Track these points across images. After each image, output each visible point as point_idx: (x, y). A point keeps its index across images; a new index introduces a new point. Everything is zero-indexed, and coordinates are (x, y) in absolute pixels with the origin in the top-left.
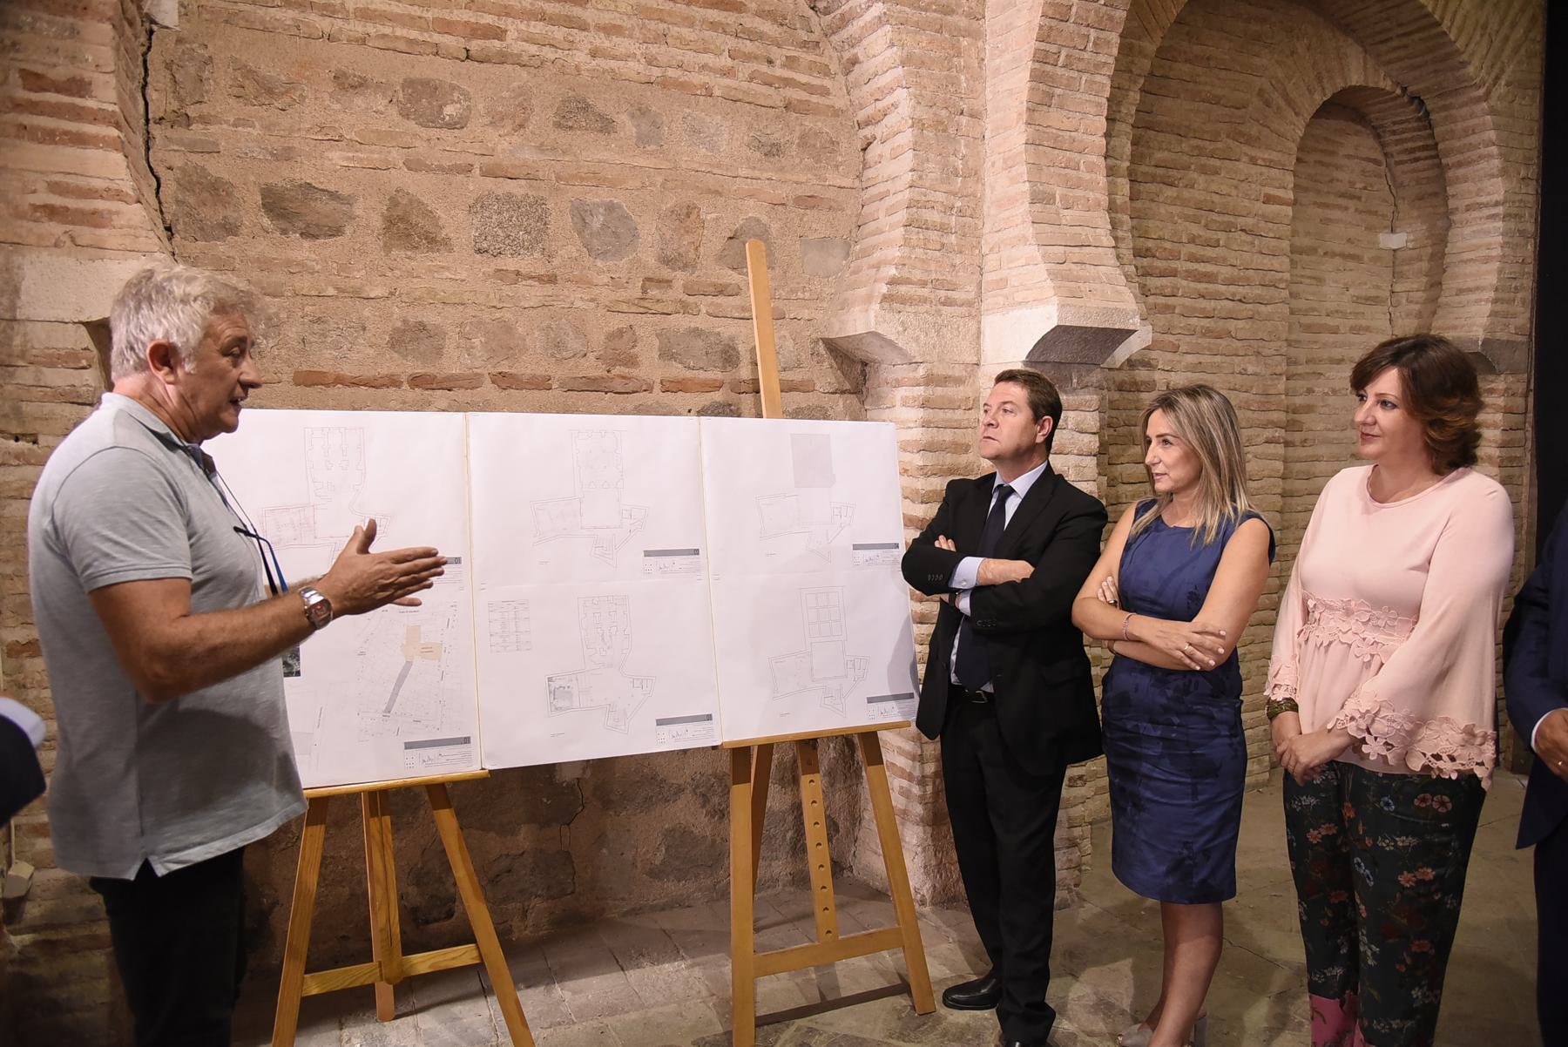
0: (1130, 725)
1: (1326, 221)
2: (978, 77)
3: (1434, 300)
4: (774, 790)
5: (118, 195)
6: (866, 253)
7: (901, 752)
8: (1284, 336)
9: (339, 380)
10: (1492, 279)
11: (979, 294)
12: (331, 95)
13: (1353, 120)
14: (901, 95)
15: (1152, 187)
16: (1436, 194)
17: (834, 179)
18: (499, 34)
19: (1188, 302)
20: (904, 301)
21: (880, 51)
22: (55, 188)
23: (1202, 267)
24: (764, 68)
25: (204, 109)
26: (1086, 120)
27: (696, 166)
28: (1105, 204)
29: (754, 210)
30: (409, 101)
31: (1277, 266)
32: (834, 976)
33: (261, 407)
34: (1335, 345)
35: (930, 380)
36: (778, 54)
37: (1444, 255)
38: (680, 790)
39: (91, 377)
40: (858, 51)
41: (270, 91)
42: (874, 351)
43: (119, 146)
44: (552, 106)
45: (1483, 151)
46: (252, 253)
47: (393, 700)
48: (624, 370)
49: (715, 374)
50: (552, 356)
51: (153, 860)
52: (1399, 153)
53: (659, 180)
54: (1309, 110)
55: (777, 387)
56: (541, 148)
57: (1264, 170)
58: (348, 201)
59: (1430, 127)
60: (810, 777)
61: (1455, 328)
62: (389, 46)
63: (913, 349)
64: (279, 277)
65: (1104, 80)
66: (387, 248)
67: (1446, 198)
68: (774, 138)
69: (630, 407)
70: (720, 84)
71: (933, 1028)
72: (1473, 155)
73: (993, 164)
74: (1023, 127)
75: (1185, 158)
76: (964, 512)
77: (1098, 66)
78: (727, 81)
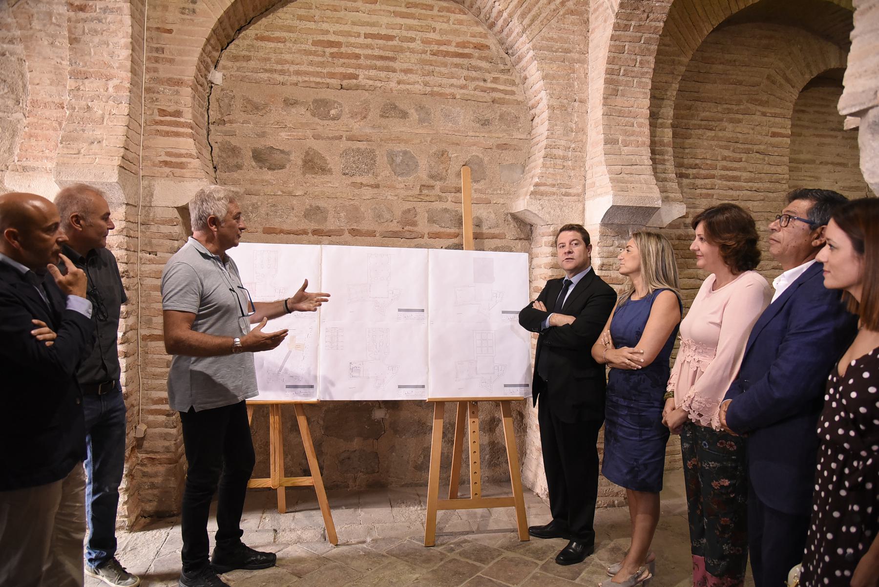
0: (615, 399)
5: (191, 156)
9: (282, 231)
14: (543, 93)
15: (700, 132)
17: (517, 135)
18: (356, 77)
19: (721, 192)
20: (542, 194)
21: (534, 72)
22: (168, 154)
23: (730, 173)
24: (482, 84)
25: (231, 117)
27: (447, 132)
29: (475, 151)
31: (780, 171)
39: (178, 230)
41: (257, 108)
43: (192, 136)
46: (248, 177)
53: (429, 139)
55: (471, 236)
56: (373, 127)
57: (771, 119)
58: (288, 154)
60: (473, 420)
62: (307, 85)
64: (258, 187)
65: (648, 81)
66: (304, 174)
75: (720, 115)
77: (643, 74)
78: (463, 91)
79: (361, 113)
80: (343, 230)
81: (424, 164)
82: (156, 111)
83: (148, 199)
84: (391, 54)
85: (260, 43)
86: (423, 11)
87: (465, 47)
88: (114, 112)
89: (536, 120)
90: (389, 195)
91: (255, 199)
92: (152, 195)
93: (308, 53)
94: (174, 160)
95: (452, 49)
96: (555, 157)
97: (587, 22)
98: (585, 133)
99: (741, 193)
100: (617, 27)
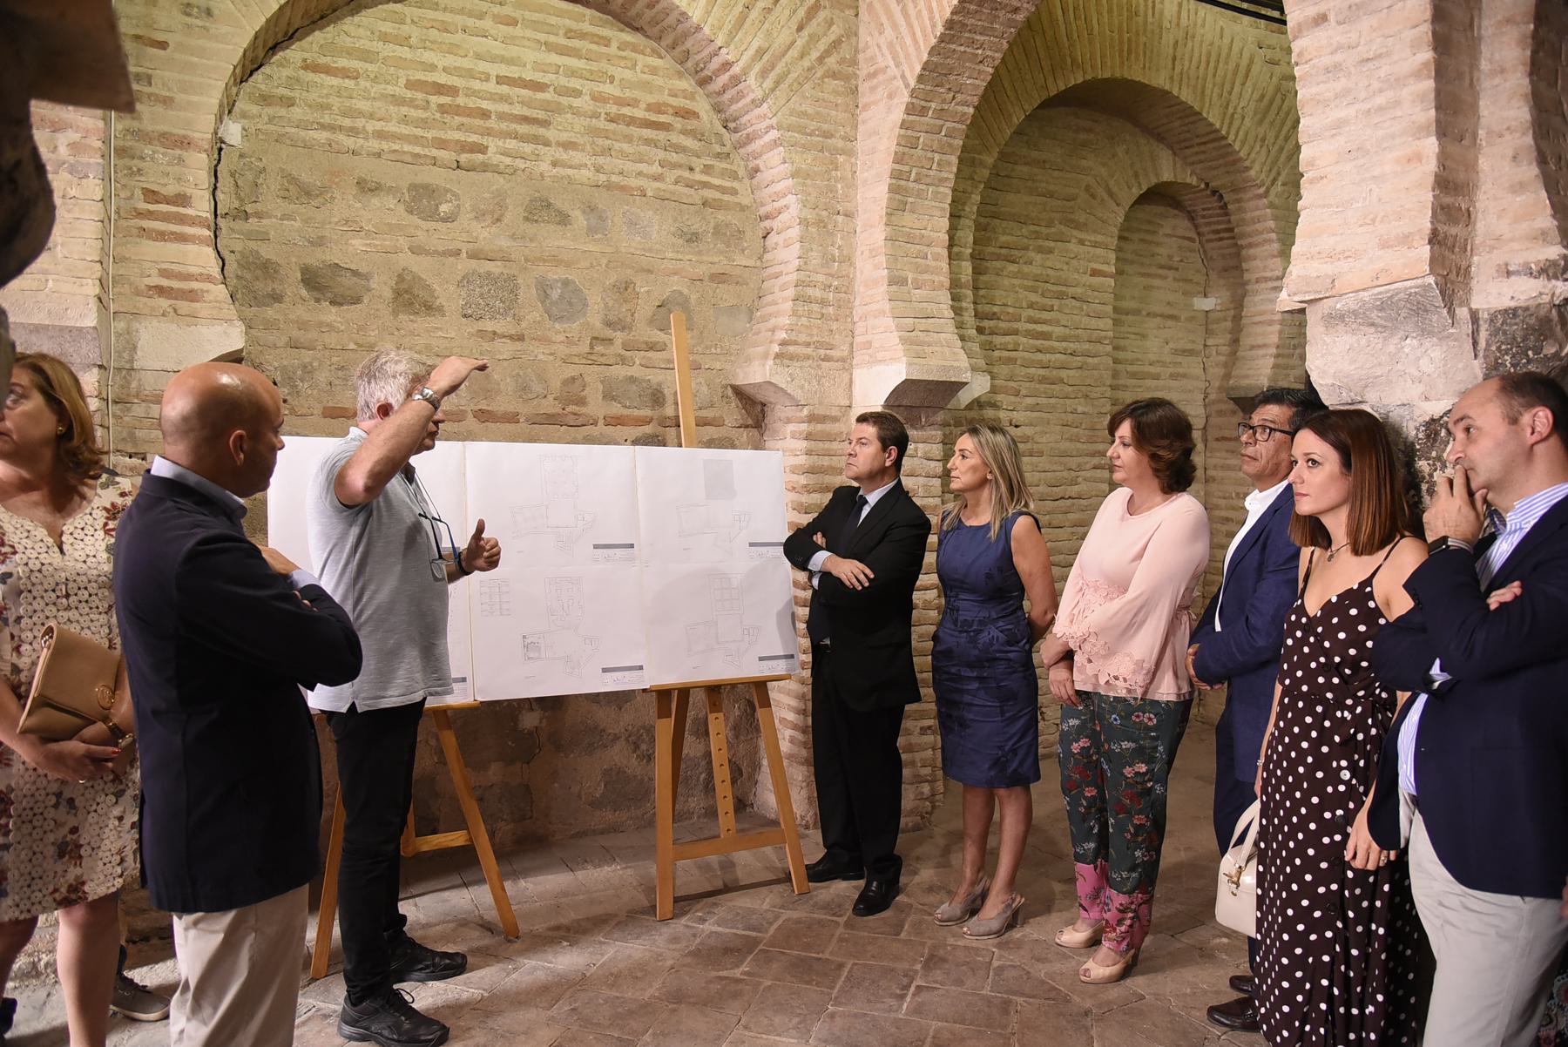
0: (953, 670)
1: (1148, 288)
2: (851, 185)
3: (1234, 353)
4: (689, 739)
5: (209, 279)
6: (764, 319)
7: (790, 708)
10: (1274, 339)
11: (851, 352)
15: (998, 264)
17: (741, 260)
21: (775, 166)
22: (164, 273)
23: (1039, 328)
24: (686, 174)
25: (259, 206)
28: (947, 284)
29: (677, 284)
31: (1101, 326)
33: (298, 434)
35: (812, 419)
36: (698, 163)
38: (616, 738)
41: (308, 194)
45: (1266, 236)
49: (646, 412)
53: (604, 261)
56: (513, 237)
58: (366, 277)
59: (1227, 214)
61: (1247, 377)
62: (398, 158)
63: (799, 395)
64: (313, 335)
65: (947, 191)
66: (395, 313)
69: (580, 437)
70: (651, 187)
72: (1259, 239)
76: (834, 521)
78: (657, 185)
79: (492, 212)
81: (596, 301)
82: (138, 192)
83: (126, 355)
84: (541, 115)
85: (310, 76)
86: (594, 47)
87: (660, 112)
88: (72, 193)
90: (540, 352)
91: (307, 356)
92: (135, 348)
93: (399, 101)
94: (175, 284)
95: (640, 113)
96: (808, 300)
97: (854, 91)
99: (1053, 357)
100: (910, 109)
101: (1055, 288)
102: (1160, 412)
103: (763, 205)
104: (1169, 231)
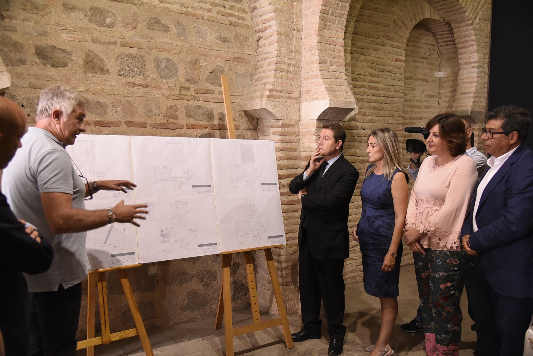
1: (416, 67)
2: (300, 17)
6: (259, 79)
8: (402, 110)
10: (474, 89)
12: (62, 11)
13: (426, 30)
14: (273, 23)
16: (455, 58)
20: (275, 97)
24: (222, 9)
26: (338, 34)
27: (198, 45)
28: (344, 64)
29: (219, 62)
30: (92, 15)
31: (399, 84)
32: (256, 339)
34: (419, 113)
35: (284, 126)
37: (457, 80)
40: (257, 4)
41: (37, 8)
42: (263, 115)
44: (146, 20)
45: (471, 43)
46: (32, 72)
47: (107, 239)
48: (173, 121)
49: (205, 123)
50: (147, 115)
51: (63, 284)
52: (442, 42)
53: (185, 50)
54: (411, 28)
56: (142, 36)
57: (395, 49)
58: (70, 53)
59: (453, 33)
61: (461, 106)
63: (277, 115)
64: (42, 82)
66: (85, 72)
67: (458, 60)
68: (227, 35)
69: (176, 134)
70: (207, 15)
71: (294, 352)
73: (305, 49)
74: (317, 36)
75: (368, 45)
80: (120, 122)
89: (262, 42)
96: (281, 71)
98: (300, 54)
101: (380, 67)
102: (451, 120)
103: (257, 25)
104: (425, 41)
